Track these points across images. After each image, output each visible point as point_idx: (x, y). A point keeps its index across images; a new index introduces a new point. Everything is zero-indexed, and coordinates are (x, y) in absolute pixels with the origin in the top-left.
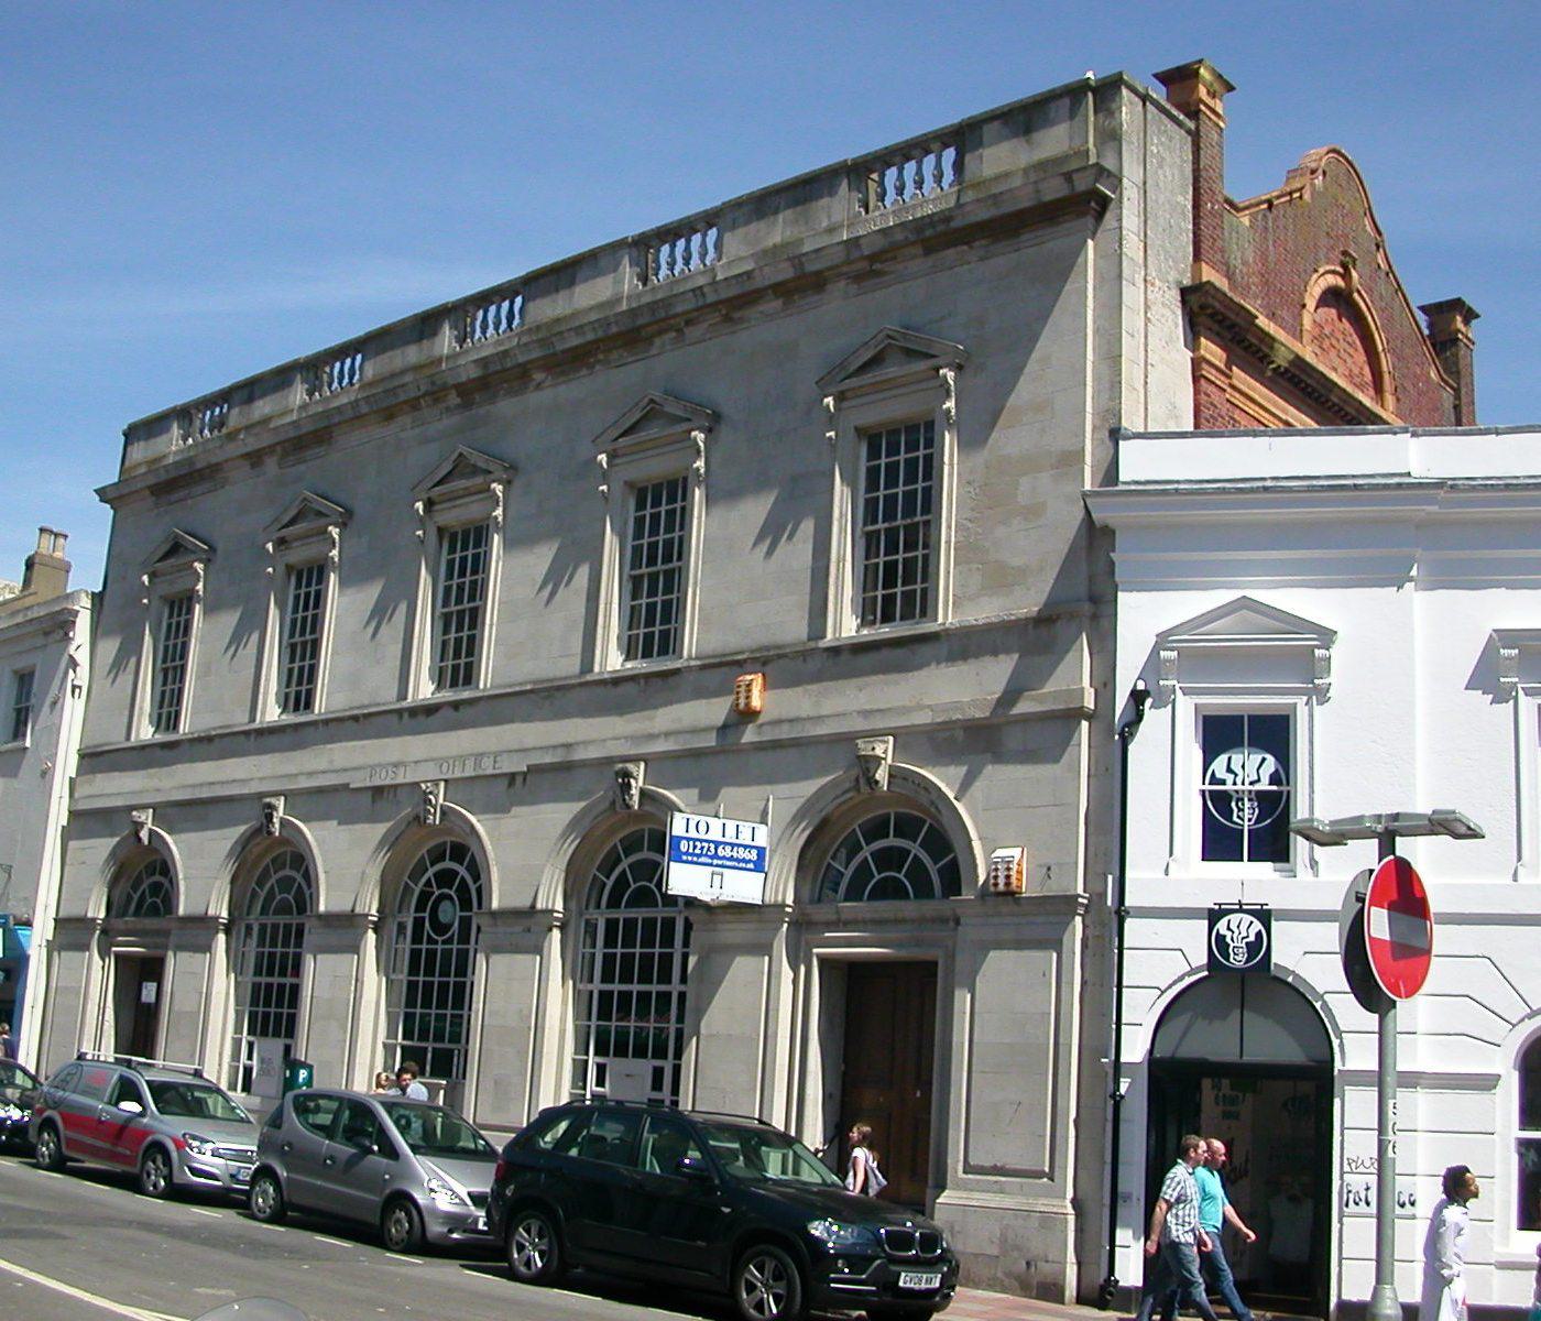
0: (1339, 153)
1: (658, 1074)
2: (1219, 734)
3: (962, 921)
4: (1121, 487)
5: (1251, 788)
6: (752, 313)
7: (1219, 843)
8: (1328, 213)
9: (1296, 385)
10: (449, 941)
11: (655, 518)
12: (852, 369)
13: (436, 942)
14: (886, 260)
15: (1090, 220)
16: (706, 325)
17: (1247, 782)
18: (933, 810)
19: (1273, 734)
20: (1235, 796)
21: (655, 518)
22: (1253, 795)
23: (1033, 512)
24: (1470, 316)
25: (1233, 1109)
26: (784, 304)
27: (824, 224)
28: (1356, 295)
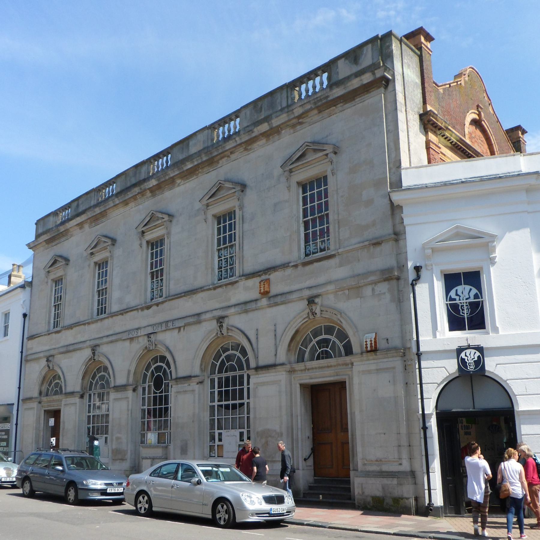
0: (473, 68)
1: (241, 434)
2: (451, 280)
3: (354, 364)
4: (403, 188)
5: (467, 301)
6: (255, 145)
7: (456, 323)
8: (471, 88)
9: (464, 153)
10: (161, 392)
11: (225, 227)
12: (294, 160)
13: (157, 393)
14: (304, 117)
15: (382, 89)
16: (237, 153)
17: (464, 299)
18: (339, 322)
19: (473, 278)
20: (460, 305)
21: (225, 227)
22: (468, 304)
23: (369, 202)
24: (524, 132)
25: (468, 431)
26: (267, 140)
27: (280, 108)
28: (483, 122)
